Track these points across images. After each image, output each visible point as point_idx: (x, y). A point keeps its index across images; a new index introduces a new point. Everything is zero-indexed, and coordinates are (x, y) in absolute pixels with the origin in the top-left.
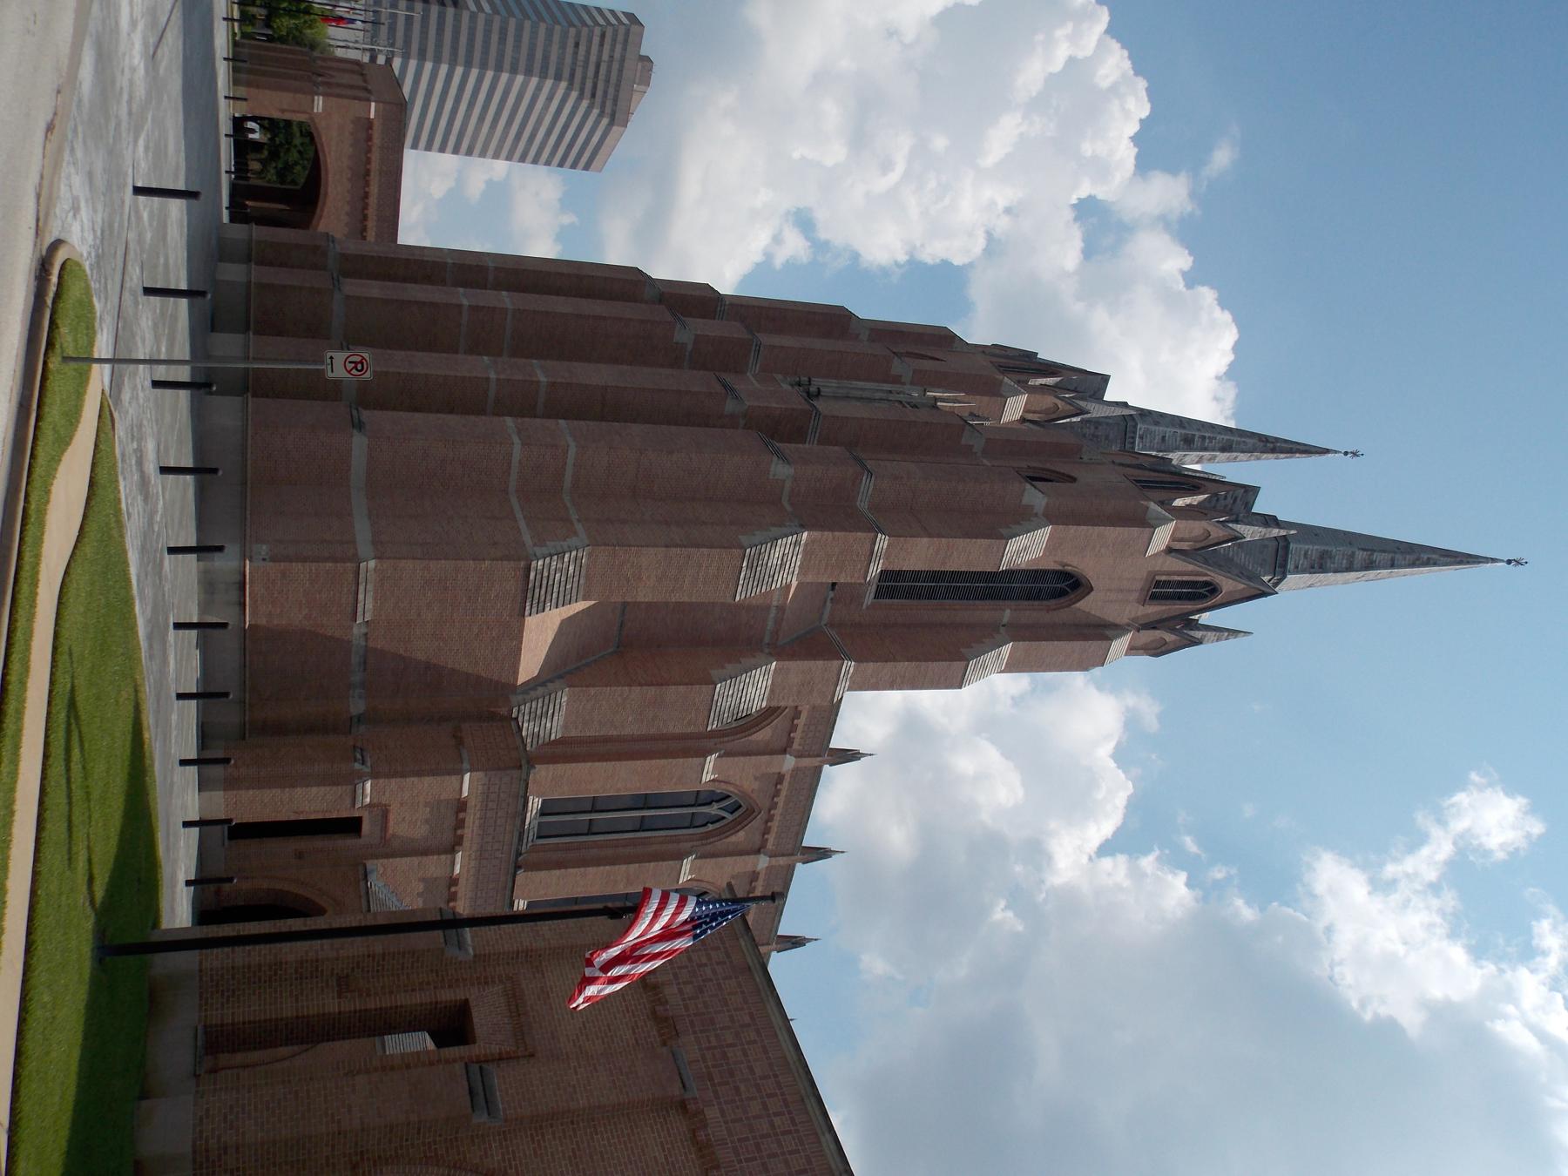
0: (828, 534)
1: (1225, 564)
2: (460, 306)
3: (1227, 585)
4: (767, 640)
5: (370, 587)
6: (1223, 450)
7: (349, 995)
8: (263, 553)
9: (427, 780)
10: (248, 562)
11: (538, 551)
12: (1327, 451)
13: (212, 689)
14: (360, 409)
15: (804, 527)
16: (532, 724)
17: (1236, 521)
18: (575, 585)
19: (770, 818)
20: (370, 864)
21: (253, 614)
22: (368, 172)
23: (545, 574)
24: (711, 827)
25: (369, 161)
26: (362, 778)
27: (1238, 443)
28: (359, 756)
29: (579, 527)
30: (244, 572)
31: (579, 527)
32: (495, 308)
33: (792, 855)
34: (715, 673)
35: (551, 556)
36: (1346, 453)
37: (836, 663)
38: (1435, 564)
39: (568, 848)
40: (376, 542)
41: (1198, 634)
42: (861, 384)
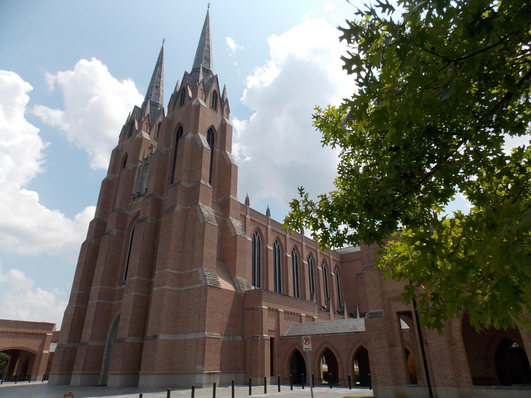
0: (200, 197)
1: (209, 87)
2: (98, 303)
3: (214, 88)
4: (223, 219)
5: (212, 334)
6: (160, 78)
7: (396, 344)
8: (200, 367)
9: (264, 318)
10: (204, 372)
11: (204, 282)
12: (162, 48)
13: (277, 382)
14: (147, 336)
15: (197, 204)
16: (245, 288)
17: (198, 80)
18: (212, 272)
19: (260, 224)
20: (281, 335)
21: (217, 370)
22: (16, 333)
23: (210, 281)
24: (260, 240)
25: (11, 332)
26: (263, 337)
27: (159, 73)
28: (256, 338)
29: (194, 270)
30: (208, 373)
31: (194, 270)
32: (100, 292)
33: (268, 219)
34: (233, 234)
35: (206, 279)
36: (163, 43)
37: (231, 200)
38: (209, 28)
39: (263, 280)
40: (198, 331)
41: (225, 99)
42: (135, 180)
